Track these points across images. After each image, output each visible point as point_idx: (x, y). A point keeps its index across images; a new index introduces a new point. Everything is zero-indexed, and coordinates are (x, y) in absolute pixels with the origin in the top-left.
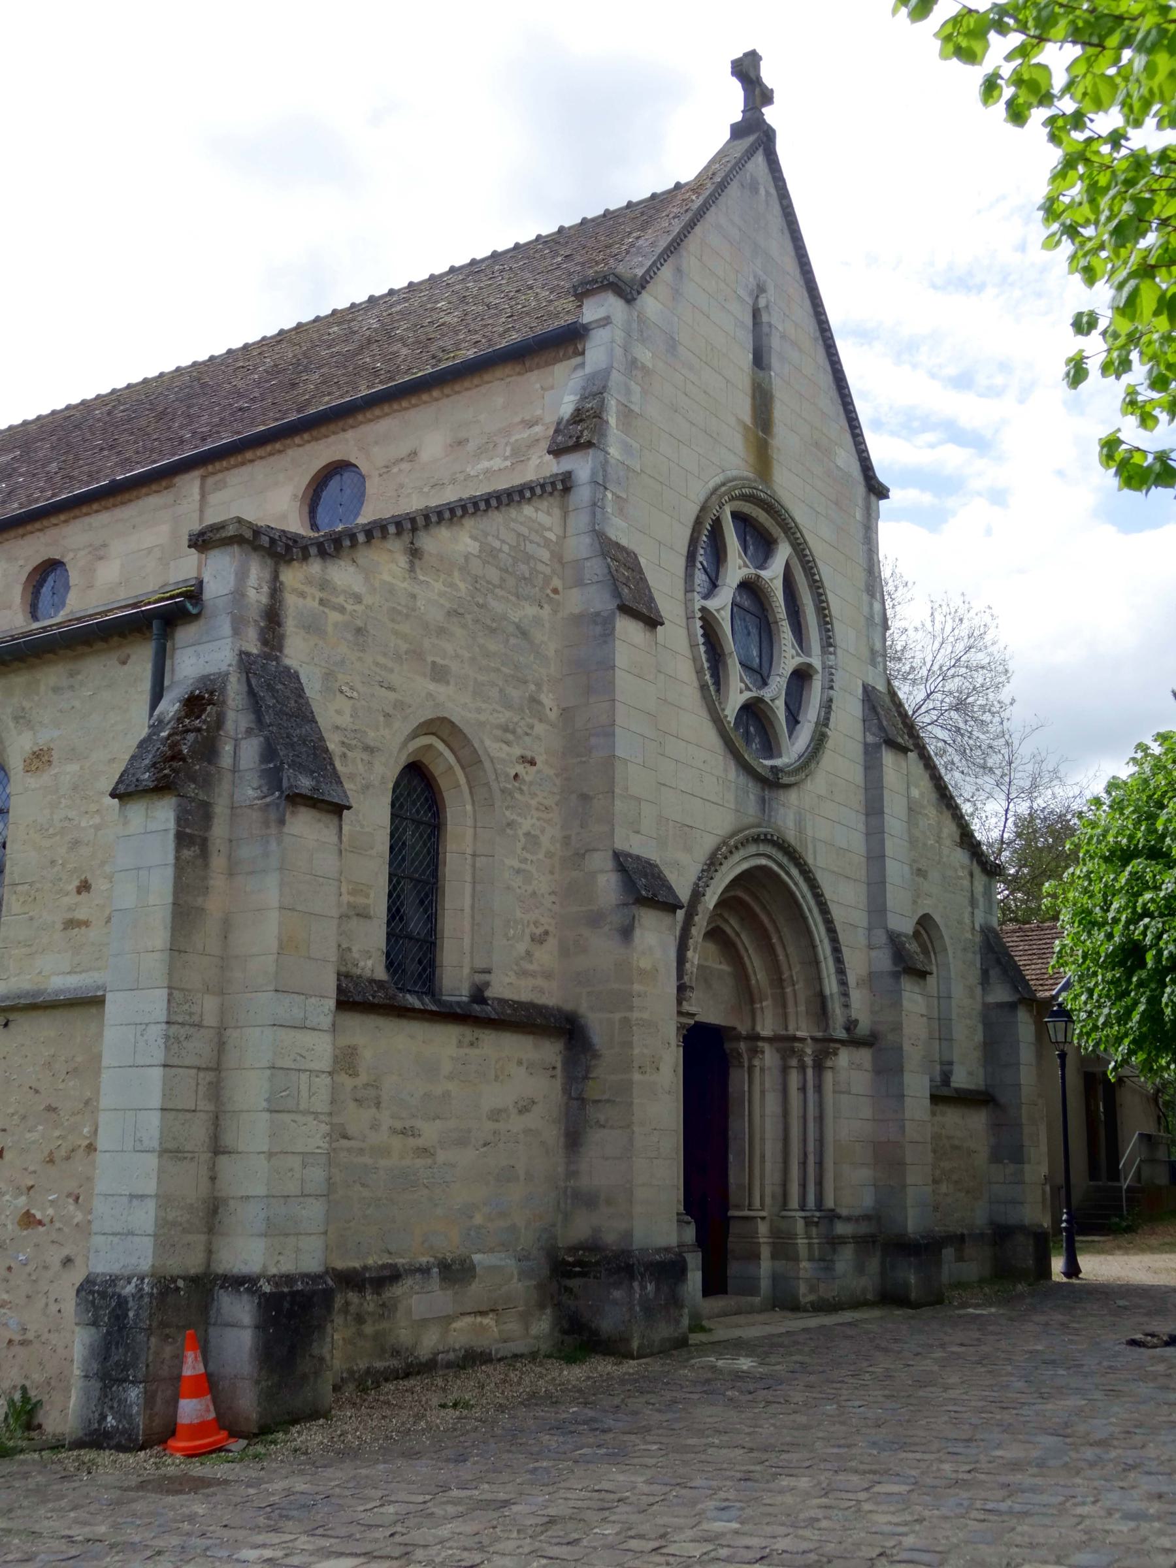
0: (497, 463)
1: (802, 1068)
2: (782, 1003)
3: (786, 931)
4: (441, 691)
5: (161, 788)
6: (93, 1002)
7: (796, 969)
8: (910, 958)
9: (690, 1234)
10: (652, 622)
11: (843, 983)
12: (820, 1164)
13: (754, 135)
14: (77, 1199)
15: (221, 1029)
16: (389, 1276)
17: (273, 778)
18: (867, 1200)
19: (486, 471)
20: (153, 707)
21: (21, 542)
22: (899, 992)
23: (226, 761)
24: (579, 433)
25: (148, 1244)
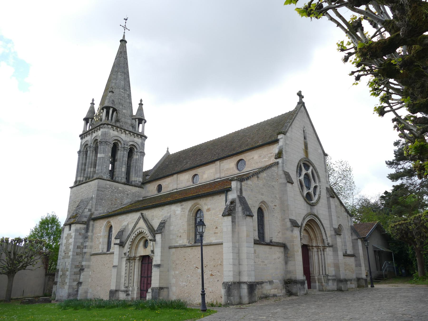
0: (266, 159)
3: (316, 229)
5: (229, 215)
7: (319, 235)
8: (338, 232)
9: (305, 278)
10: (292, 183)
11: (326, 237)
12: (325, 267)
13: (301, 104)
15: (239, 247)
16: (262, 283)
17: (244, 213)
18: (333, 273)
20: (226, 203)
22: (336, 238)
23: (237, 210)
24: (279, 155)
25: (232, 277)
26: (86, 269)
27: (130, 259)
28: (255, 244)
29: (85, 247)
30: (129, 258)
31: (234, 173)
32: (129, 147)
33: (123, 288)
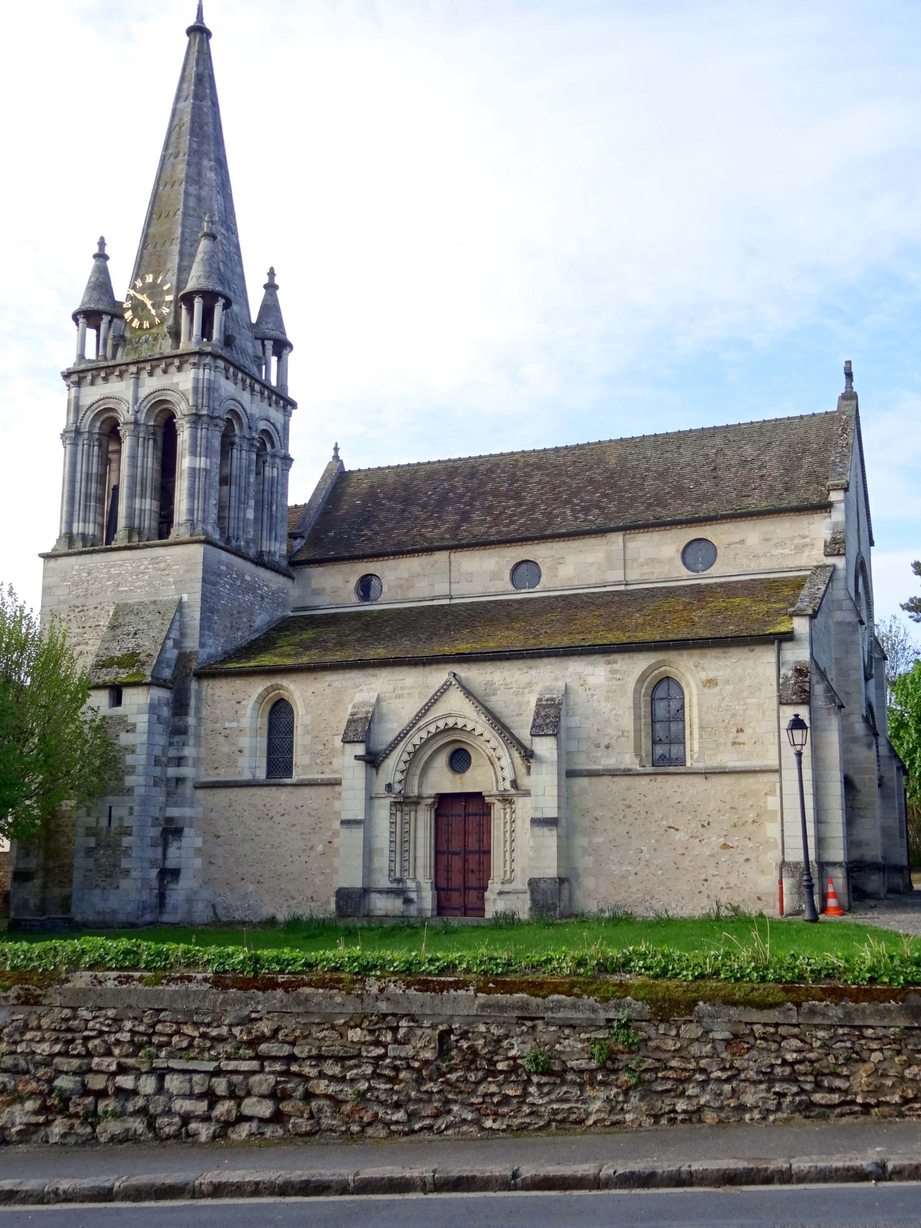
0: (787, 551)
19: (782, 554)
21: (506, 549)
27: (405, 803)
29: (180, 761)
31: (675, 575)
33: (384, 882)
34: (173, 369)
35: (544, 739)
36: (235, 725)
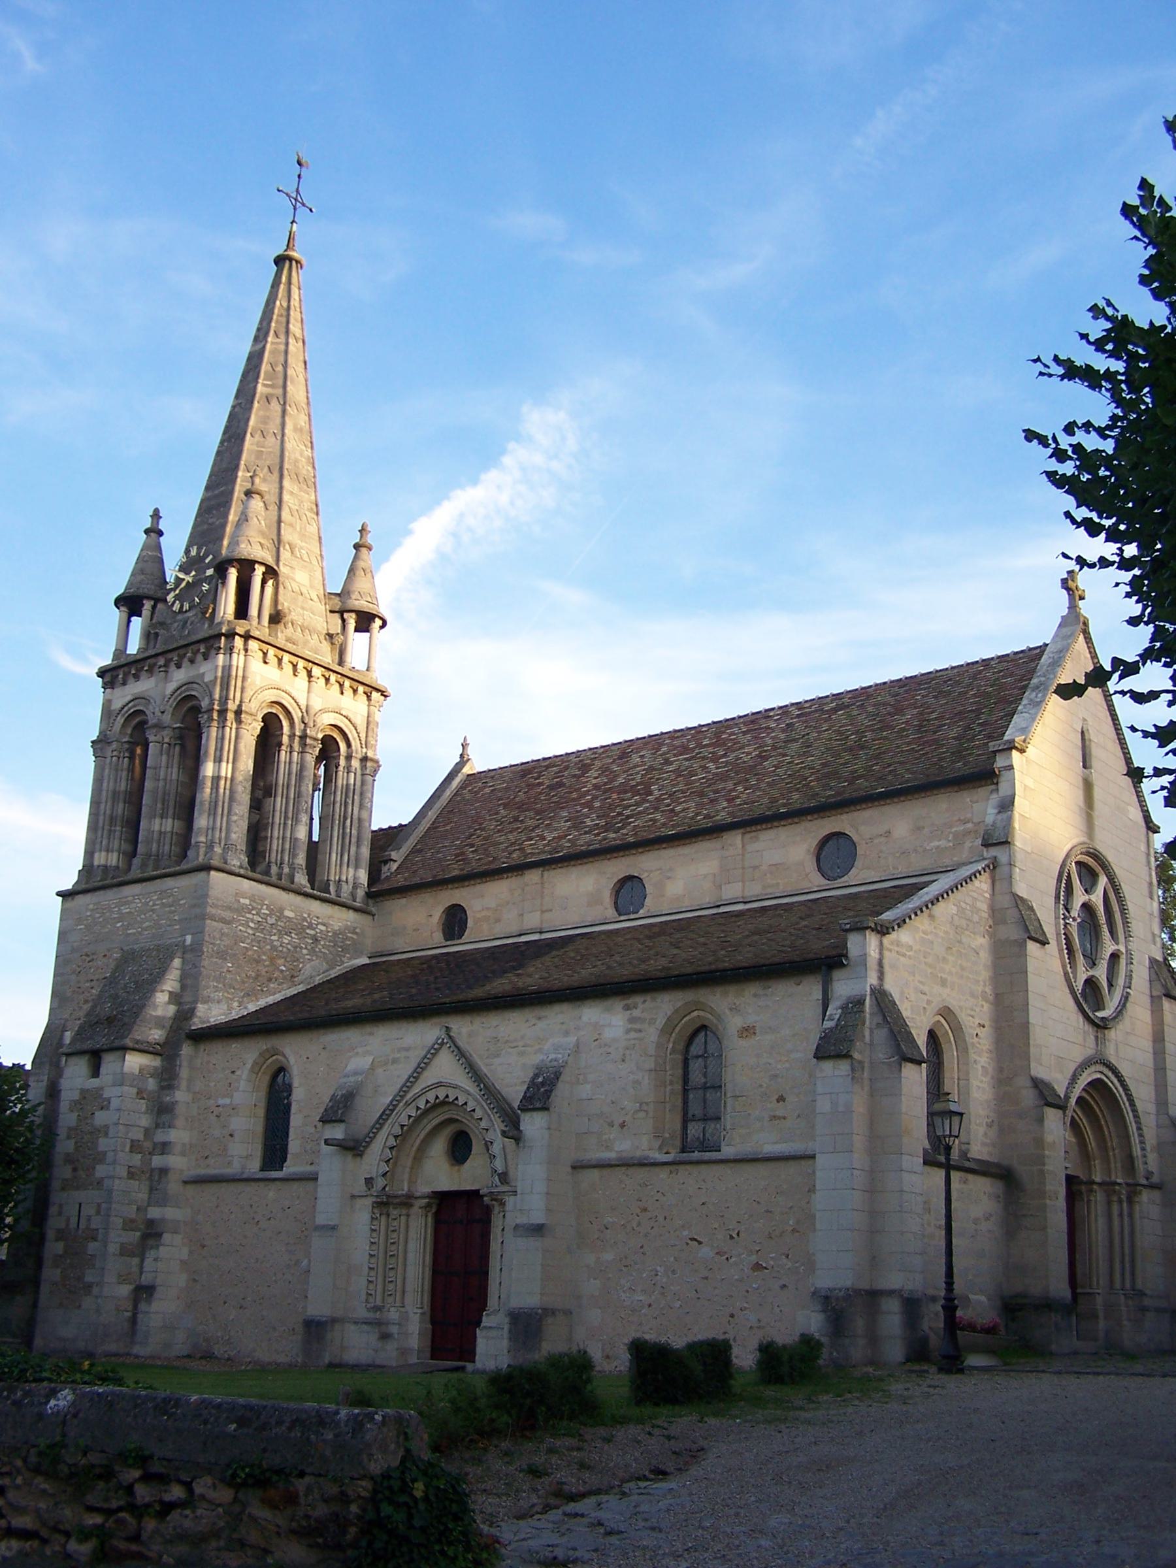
0: (943, 843)
1: (1120, 1202)
2: (1106, 1160)
4: (945, 992)
6: (813, 1157)
11: (1143, 1149)
12: (1133, 1261)
14: (787, 1256)
26: (167, 1237)
27: (387, 1204)
28: (925, 1163)
29: (164, 1148)
30: (388, 1196)
31: (805, 885)
32: (320, 736)
33: (362, 1313)
34: (200, 657)
35: (535, 1114)
36: (227, 1101)
